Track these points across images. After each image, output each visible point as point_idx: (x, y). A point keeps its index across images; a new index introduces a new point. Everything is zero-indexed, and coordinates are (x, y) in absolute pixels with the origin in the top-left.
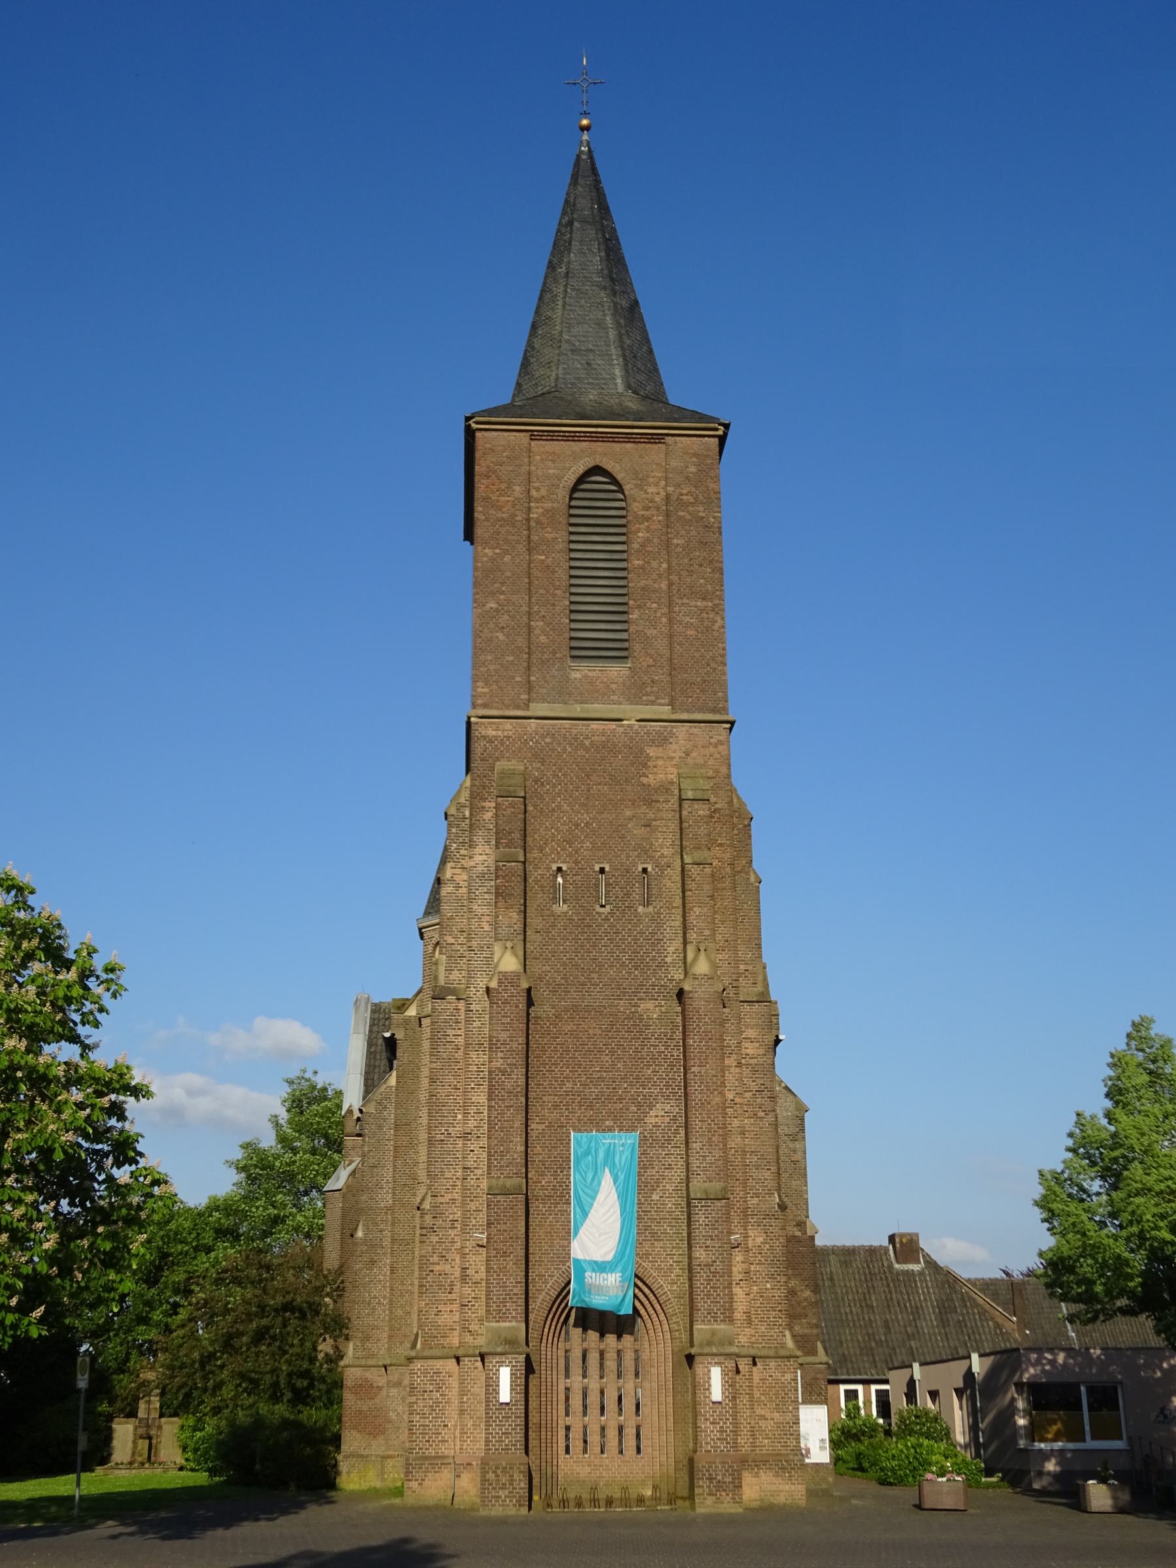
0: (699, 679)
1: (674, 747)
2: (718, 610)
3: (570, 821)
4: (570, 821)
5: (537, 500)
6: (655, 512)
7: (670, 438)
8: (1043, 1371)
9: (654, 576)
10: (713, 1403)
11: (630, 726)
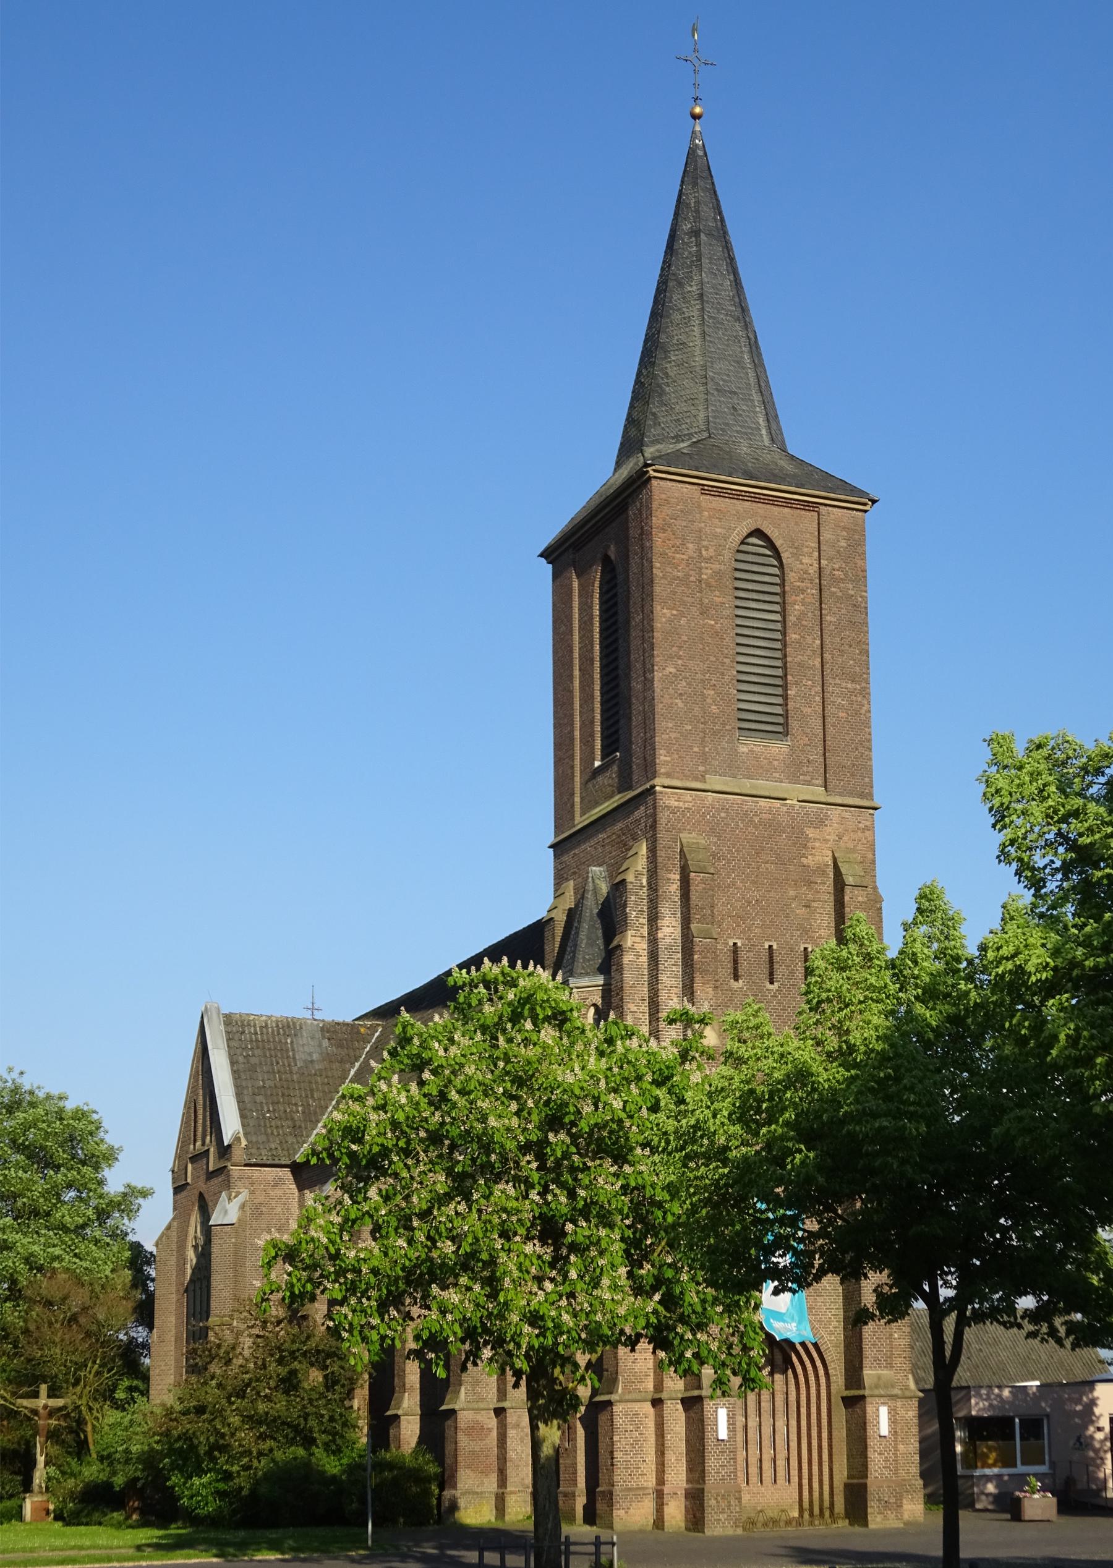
0: (849, 763)
1: (829, 829)
2: (865, 693)
3: (743, 898)
4: (743, 898)
5: (708, 560)
6: (809, 585)
7: (824, 507)
8: (991, 1405)
9: (809, 652)
10: (880, 1436)
11: (792, 806)
